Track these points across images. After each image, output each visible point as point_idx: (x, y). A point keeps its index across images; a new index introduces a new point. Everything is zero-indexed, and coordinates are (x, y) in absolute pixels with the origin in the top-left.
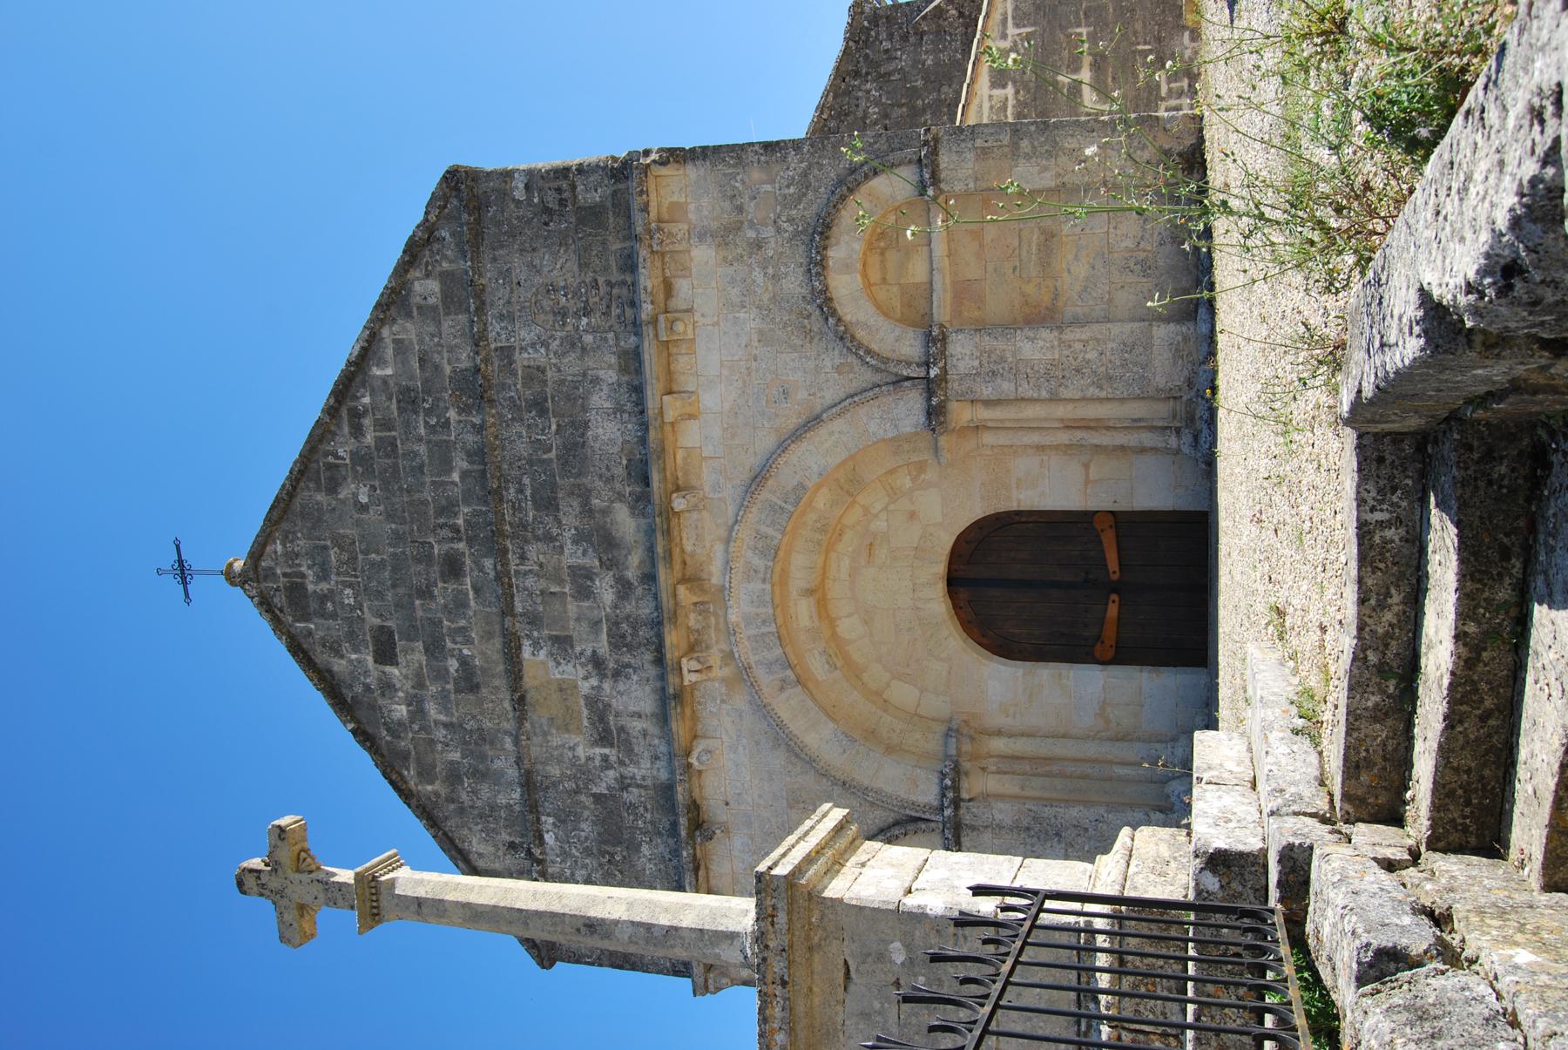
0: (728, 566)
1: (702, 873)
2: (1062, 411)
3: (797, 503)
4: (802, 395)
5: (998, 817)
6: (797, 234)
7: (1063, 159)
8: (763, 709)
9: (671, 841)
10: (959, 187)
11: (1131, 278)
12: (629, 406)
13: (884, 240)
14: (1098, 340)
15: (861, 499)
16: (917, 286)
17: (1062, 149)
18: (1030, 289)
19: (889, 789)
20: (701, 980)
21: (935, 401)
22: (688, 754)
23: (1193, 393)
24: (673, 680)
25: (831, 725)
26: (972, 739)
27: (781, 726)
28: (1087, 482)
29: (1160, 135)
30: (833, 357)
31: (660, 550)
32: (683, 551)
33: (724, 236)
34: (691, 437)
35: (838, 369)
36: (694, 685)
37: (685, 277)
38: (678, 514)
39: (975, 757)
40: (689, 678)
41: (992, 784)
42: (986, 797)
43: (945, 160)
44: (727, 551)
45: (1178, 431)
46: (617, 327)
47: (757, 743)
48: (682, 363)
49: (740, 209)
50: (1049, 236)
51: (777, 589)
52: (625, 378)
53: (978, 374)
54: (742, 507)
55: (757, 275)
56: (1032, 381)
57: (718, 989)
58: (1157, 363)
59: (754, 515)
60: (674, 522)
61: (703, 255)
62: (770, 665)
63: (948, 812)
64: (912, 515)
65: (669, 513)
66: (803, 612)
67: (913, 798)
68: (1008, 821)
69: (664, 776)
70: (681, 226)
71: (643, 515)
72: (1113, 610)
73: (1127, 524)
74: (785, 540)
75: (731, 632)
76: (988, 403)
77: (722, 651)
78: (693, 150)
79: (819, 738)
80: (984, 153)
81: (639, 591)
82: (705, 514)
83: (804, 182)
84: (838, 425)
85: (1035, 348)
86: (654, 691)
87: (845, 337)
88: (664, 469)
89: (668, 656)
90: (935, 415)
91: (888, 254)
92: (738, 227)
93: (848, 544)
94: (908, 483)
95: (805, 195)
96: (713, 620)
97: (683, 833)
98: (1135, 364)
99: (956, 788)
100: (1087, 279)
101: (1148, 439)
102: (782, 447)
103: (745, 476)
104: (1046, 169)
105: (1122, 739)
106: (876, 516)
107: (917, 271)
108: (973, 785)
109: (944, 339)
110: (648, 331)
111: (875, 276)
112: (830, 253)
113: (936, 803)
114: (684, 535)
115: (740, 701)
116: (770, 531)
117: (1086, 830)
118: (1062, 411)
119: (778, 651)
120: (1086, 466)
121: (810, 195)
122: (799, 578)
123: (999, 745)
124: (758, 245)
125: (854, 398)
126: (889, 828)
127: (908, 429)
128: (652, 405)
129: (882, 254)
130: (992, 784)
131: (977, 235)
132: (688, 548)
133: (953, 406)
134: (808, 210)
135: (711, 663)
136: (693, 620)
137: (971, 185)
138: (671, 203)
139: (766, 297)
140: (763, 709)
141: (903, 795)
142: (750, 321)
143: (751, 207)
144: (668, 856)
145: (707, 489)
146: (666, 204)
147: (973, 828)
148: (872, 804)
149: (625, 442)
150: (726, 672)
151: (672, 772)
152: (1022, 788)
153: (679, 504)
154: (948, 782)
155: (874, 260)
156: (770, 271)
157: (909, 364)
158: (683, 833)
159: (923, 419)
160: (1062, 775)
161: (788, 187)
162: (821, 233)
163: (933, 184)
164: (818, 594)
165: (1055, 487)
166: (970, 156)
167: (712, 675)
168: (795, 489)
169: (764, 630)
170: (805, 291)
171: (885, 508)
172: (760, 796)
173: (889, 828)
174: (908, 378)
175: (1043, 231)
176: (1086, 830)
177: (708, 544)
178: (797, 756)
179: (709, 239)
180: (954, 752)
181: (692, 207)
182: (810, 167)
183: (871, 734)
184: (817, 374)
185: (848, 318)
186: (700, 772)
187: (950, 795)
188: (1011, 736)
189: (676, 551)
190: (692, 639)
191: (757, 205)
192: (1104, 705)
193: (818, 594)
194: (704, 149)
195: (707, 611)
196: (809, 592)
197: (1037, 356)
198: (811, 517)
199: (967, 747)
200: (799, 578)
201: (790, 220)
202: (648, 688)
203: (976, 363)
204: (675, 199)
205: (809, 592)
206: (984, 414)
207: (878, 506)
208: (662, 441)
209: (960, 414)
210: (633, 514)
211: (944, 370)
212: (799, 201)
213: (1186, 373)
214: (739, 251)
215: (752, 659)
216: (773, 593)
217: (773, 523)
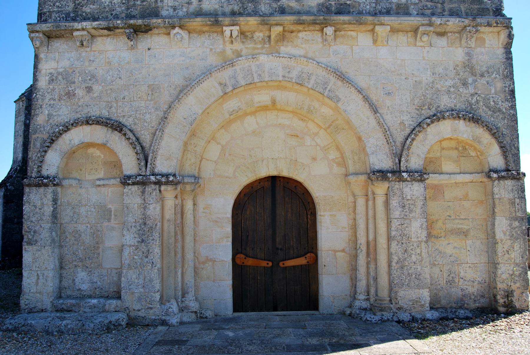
0: (291, 57)
1: (106, 32)
2: (382, 241)
3: (329, 98)
4: (388, 103)
5: (151, 207)
6: (471, 104)
7: (509, 243)
8: (208, 73)
9: (123, 15)
10: (496, 190)
11: (445, 275)
12: (379, 7)
13: (462, 148)
14: (421, 261)
15: (322, 132)
16: (440, 166)
17: (514, 242)
18: (440, 224)
19: (163, 143)
20: (38, 29)
21: (389, 175)
22: (181, 27)
23: (395, 310)
24: (227, 20)
25: (200, 112)
26: (193, 191)
27: (199, 82)
28: (335, 251)
29: (520, 291)
30: (410, 123)
31: (304, 17)
32: (299, 31)
33: (469, 66)
34: (363, 39)
35: (402, 123)
36: (222, 32)
37: (448, 44)
38: (322, 30)
39: (182, 192)
40: (227, 30)
41: (170, 203)
42: (162, 200)
43: (509, 183)
44: (300, 56)
45: (368, 300)
46: (421, 4)
47: (187, 68)
48: (402, 38)
49: (482, 75)
50: (465, 234)
51: (276, 84)
52: (394, 7)
53: (403, 198)
54: (327, 68)
55: (449, 83)
56: (400, 227)
57: (32, 39)
58: (410, 291)
59: (322, 73)
60: (318, 27)
61: (459, 54)
62: (234, 77)
63: (153, 178)
64: (314, 159)
65: (325, 24)
66: (263, 97)
67: (159, 158)
68: (149, 213)
69: (164, 13)
70: (474, 43)
71: (319, 11)
72: (264, 264)
73: (310, 273)
74: (305, 90)
75: (254, 57)
76: (387, 203)
77: (241, 51)
78: (510, 53)
79: (191, 105)
80: (513, 203)
81: (275, 5)
82: (321, 45)
83: (496, 110)
84: (373, 122)
85: (416, 228)
86: (215, 10)
87: (419, 127)
88: (350, 23)
89: (241, 19)
90: (382, 175)
91: (456, 152)
92: (473, 74)
93: (297, 124)
94: (331, 157)
95: (490, 110)
96: (259, 46)
97: (132, 22)
98: (409, 281)
99: (167, 183)
100: (445, 253)
101: (362, 285)
102: (360, 91)
103: (343, 70)
104: (505, 234)
105: (195, 272)
106: (313, 140)
107: (447, 166)
108: (169, 192)
109: (422, 180)
110: (426, 21)
111: (445, 144)
112: (462, 122)
113: (156, 171)
114: (308, 33)
115: (213, 60)
116: (312, 81)
117: (147, 257)
118: (382, 241)
119: (243, 83)
120: (343, 251)
121: (490, 113)
122: (281, 96)
123: (189, 205)
124: (465, 84)
125: (387, 132)
126: (140, 144)
127: (371, 160)
128: (386, 19)
129: (456, 149)
130: (170, 203)
131: (466, 197)
132: (301, 35)
133: (386, 185)
134: (483, 112)
135: (235, 44)
136: (259, 35)
137: (497, 196)
138: (484, 39)
139: (439, 86)
140: (208, 73)
141: (160, 152)
142: (426, 77)
143: (483, 81)
144: (114, 13)
145: (335, 47)
146: (484, 36)
147: (143, 192)
148: (154, 134)
149: (359, 4)
150: (229, 53)
151: (166, 17)
152: (168, 220)
153: (329, 30)
154: (171, 178)
155: (453, 144)
156: (452, 89)
157: (407, 161)
158: (132, 22)
159: (377, 168)
160: (176, 241)
161: (494, 101)
162: (473, 118)
163: (499, 177)
164: (273, 106)
165: (331, 234)
166: (511, 196)
167: (228, 44)
168: (337, 96)
169: (255, 75)
170: (442, 107)
171: (317, 145)
172: (154, 69)
173: (140, 144)
174: (400, 161)
175: (468, 231)
176: (147, 257)
177: (303, 46)
178: (181, 91)
179: (467, 58)
180: (186, 180)
181: (483, 50)
182: (503, 113)
183: (193, 134)
184: (400, 113)
185: (429, 129)
186: (169, 34)
187: (163, 180)
188: (194, 210)
189: (300, 27)
190: (248, 34)
191: (484, 84)
192: (213, 261)
193: (273, 106)
194: (511, 59)
195: (265, 43)
196: (274, 102)
197: (413, 229)
198: (316, 104)
199: (188, 188)
200: (281, 96)
201: (477, 102)
202: (217, 6)
203: (409, 197)
204: (487, 42)
205: (274, 102)
206: (380, 201)
207: (319, 141)
208: (366, 24)
209: (381, 189)
210: (319, 5)
211: (406, 180)
212: (487, 107)
213: (405, 306)
214: (461, 74)
215: (237, 68)
216: (276, 81)
217: (317, 83)
